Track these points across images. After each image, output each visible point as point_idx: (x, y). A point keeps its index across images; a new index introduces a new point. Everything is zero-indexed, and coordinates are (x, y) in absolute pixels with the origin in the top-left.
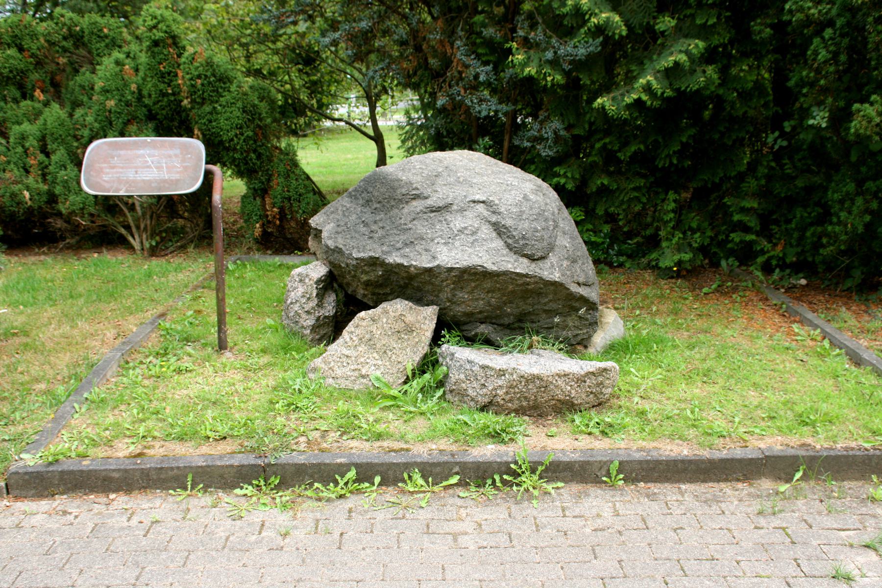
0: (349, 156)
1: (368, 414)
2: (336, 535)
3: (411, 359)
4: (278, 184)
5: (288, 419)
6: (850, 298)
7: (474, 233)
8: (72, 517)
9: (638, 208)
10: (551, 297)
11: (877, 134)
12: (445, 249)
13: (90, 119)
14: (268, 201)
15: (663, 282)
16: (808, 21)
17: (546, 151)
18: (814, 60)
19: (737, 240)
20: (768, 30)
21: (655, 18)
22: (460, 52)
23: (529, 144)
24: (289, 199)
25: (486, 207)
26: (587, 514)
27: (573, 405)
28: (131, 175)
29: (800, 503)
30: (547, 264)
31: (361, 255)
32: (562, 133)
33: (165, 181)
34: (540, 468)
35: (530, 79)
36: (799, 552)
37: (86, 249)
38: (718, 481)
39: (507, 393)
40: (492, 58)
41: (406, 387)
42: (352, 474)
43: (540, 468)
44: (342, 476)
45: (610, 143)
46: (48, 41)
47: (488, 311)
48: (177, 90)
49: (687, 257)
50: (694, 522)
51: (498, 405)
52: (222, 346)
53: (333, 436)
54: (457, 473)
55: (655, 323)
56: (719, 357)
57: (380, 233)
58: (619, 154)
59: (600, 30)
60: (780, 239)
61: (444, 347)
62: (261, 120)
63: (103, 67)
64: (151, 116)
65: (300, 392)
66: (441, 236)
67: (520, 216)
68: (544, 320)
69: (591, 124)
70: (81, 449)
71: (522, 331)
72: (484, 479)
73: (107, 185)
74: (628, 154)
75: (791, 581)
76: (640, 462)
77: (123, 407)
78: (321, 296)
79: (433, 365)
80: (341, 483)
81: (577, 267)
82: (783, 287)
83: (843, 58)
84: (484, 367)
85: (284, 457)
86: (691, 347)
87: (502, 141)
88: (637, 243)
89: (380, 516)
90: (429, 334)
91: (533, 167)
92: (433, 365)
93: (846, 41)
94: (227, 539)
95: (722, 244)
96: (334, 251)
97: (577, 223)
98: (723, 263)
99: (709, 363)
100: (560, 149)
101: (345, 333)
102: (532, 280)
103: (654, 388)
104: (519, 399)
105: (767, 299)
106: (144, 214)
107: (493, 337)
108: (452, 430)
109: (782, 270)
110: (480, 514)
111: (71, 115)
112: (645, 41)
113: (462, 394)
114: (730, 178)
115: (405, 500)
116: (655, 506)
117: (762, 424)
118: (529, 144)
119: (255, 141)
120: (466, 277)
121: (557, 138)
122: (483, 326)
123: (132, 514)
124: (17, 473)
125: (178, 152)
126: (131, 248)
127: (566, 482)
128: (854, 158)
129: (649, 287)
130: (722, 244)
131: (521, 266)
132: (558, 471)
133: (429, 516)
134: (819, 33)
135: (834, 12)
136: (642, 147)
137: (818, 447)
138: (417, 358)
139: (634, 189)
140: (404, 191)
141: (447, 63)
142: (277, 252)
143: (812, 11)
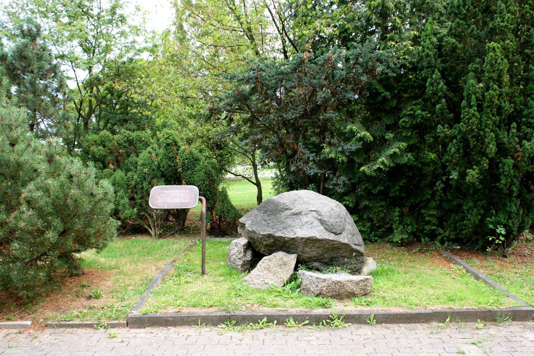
0: (240, 193)
1: (270, 298)
2: (261, 340)
3: (286, 276)
4: (219, 205)
5: (236, 300)
6: (478, 254)
7: (311, 224)
8: (155, 334)
9: (382, 215)
10: (344, 250)
11: (478, 182)
12: (300, 230)
13: (135, 177)
14: (214, 213)
15: (395, 248)
16: (446, 137)
17: (340, 190)
18: (450, 152)
19: (428, 229)
20: (432, 139)
21: (385, 133)
22: (301, 147)
23: (332, 187)
24: (223, 212)
25: (315, 213)
26: (361, 334)
27: (355, 294)
28: (169, 200)
29: (448, 330)
30: (342, 236)
31: (264, 233)
32: (346, 182)
33: (183, 203)
34: (342, 317)
35: (332, 159)
36: (445, 345)
37: (129, 235)
38: (415, 323)
39: (327, 289)
40: (314, 150)
41: (284, 288)
42: (265, 319)
43: (342, 317)
44: (261, 320)
45: (368, 186)
46: (118, 143)
47: (318, 256)
48: (176, 164)
49: (405, 236)
50: (404, 336)
51: (323, 294)
52: (203, 273)
53: (256, 306)
54: (308, 320)
55: (391, 264)
56: (417, 276)
57: (272, 224)
58: (372, 191)
59: (361, 139)
60: (447, 228)
61: (300, 271)
62: (212, 177)
63: (143, 154)
64: (163, 176)
65: (240, 290)
66: (298, 225)
67: (330, 216)
68: (341, 260)
69: (359, 178)
70: (155, 310)
71: (332, 265)
72: (319, 322)
73: (160, 205)
74: (377, 191)
75: (441, 354)
76: (383, 315)
77: (167, 295)
78: (245, 252)
79: (295, 279)
80: (261, 323)
81: (355, 238)
82: (449, 249)
83: (461, 151)
84: (317, 278)
85: (237, 313)
86: (406, 273)
87: (320, 185)
88: (383, 231)
89: (278, 335)
90: (293, 266)
91: (334, 197)
92: (295, 279)
93: (462, 144)
94: (219, 341)
95: (422, 231)
96: (251, 232)
97: (355, 222)
98: (423, 240)
99: (413, 279)
100: (346, 189)
101: (258, 265)
102: (336, 243)
103: (389, 289)
104: (332, 291)
105: (441, 255)
106: (157, 219)
107: (320, 268)
108: (305, 303)
109: (449, 241)
110: (318, 334)
111: (126, 175)
112: (380, 143)
113: (308, 290)
114: (423, 201)
115: (287, 329)
116: (389, 331)
117: (434, 301)
118: (332, 187)
119: (209, 186)
120: (309, 241)
121: (345, 184)
122: (315, 263)
123: (179, 333)
124: (131, 318)
125: (188, 191)
126: (150, 235)
127: (353, 324)
128: (471, 192)
129: (388, 250)
130: (422, 231)
131: (332, 237)
132: (349, 319)
133: (298, 335)
134: (451, 141)
135: (456, 133)
136: (383, 188)
137: (456, 308)
138: (289, 276)
139: (381, 206)
140: (282, 207)
141: (295, 152)
142: (217, 236)
143: (448, 132)
